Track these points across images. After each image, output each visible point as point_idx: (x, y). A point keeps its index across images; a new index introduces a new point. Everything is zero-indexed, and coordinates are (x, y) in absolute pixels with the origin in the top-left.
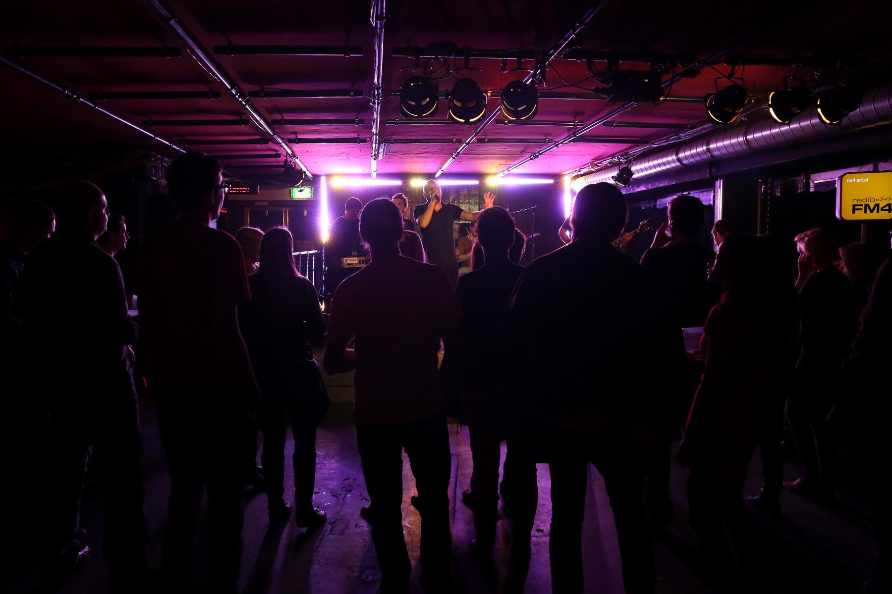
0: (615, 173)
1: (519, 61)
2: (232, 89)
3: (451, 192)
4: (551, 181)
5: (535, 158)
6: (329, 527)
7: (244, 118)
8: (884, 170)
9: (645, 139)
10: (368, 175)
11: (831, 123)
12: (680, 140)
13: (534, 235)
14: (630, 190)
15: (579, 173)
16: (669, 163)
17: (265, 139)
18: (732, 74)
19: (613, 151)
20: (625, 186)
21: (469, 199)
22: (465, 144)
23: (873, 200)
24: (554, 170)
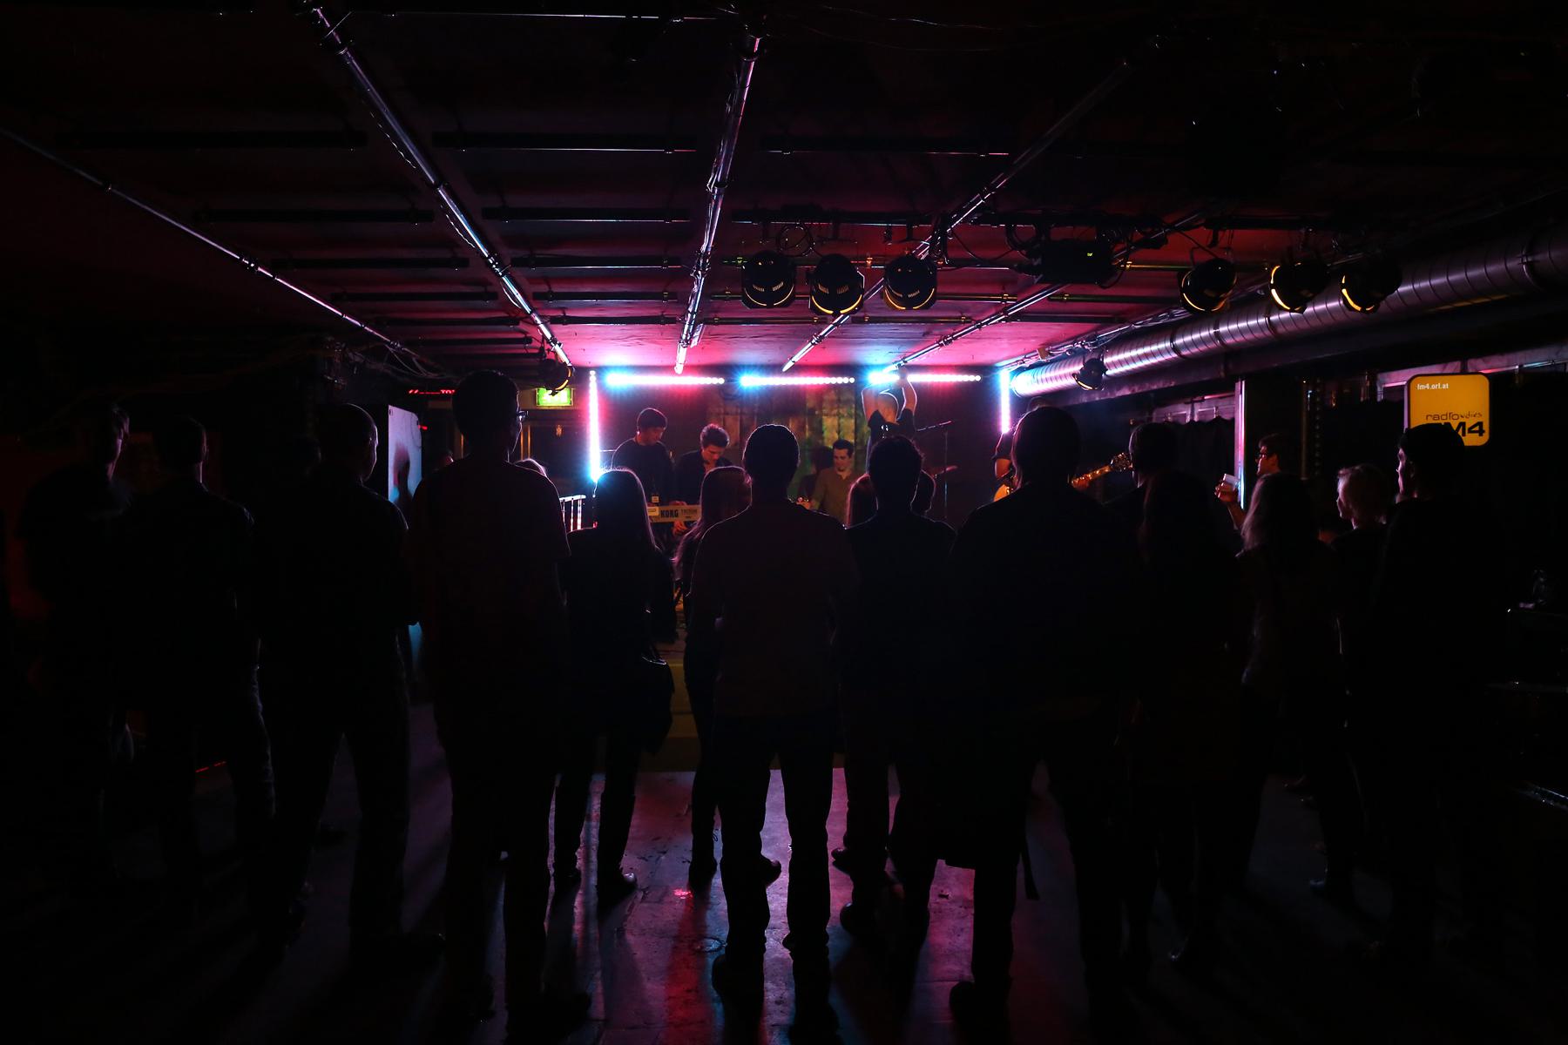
0: (1077, 368)
1: (909, 228)
2: (489, 257)
3: (808, 397)
4: (978, 378)
5: (946, 343)
6: (640, 895)
7: (490, 289)
8: (1474, 371)
9: (1123, 316)
10: (669, 369)
11: (1363, 310)
12: (1173, 320)
13: (947, 469)
14: (1106, 395)
15: (1023, 365)
16: (1160, 352)
17: (517, 316)
18: (1214, 243)
19: (1083, 331)
20: (1094, 389)
21: (838, 407)
22: (831, 326)
23: (1456, 417)
24: (982, 358)
